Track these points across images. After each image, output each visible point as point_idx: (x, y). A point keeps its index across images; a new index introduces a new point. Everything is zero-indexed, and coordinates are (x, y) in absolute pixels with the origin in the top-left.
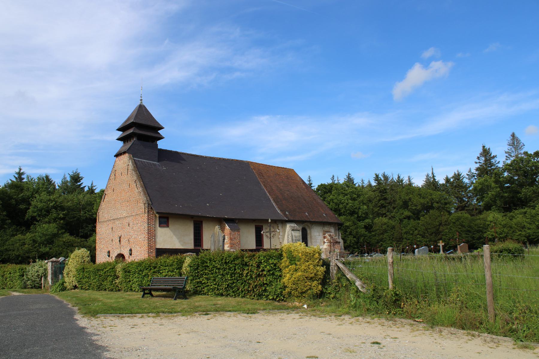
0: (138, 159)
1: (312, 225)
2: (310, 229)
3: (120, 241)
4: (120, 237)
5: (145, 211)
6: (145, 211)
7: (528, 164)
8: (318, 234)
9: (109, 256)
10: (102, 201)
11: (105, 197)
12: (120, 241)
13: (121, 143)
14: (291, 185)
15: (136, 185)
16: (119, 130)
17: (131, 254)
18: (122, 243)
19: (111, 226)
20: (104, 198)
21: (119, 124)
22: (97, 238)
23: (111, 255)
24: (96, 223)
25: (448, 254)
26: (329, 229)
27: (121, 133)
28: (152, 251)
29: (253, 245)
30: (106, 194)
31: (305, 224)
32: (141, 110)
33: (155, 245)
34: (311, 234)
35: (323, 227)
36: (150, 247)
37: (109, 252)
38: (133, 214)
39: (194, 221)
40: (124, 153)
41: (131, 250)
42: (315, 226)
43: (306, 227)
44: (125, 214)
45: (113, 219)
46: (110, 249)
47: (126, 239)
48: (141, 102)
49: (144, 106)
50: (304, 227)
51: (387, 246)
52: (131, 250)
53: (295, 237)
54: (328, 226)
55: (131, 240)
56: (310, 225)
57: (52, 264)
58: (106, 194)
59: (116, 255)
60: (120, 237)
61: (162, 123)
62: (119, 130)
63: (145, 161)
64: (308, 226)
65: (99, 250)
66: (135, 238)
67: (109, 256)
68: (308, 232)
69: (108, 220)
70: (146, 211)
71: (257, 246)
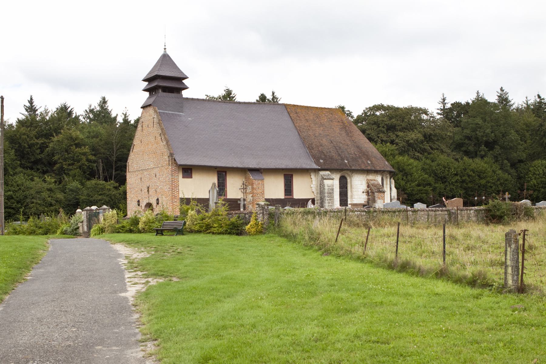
0: (163, 111)
1: (352, 173)
2: (350, 177)
3: (148, 191)
4: (148, 188)
5: (169, 163)
6: (169, 163)
7: (436, 141)
8: (360, 183)
9: (139, 205)
10: (131, 151)
11: (133, 147)
12: (148, 191)
13: (147, 94)
14: (333, 129)
15: (161, 138)
16: (145, 80)
17: (158, 204)
18: (150, 193)
19: (139, 176)
20: (133, 149)
21: (144, 75)
22: (127, 187)
23: (141, 204)
24: (126, 173)
25: (431, 208)
26: (374, 177)
27: (147, 83)
28: (176, 200)
29: (280, 194)
30: (134, 145)
31: (343, 172)
32: (165, 59)
33: (179, 196)
34: (351, 183)
35: (367, 175)
36: (174, 197)
37: (139, 201)
38: (159, 166)
39: (218, 172)
40: (150, 105)
41: (158, 200)
42: (356, 174)
43: (346, 176)
44: (152, 166)
45: (142, 170)
46: (140, 198)
47: (153, 189)
48: (165, 52)
49: (168, 56)
50: (343, 175)
51: (417, 197)
52: (158, 200)
53: (328, 187)
54: (373, 174)
55: (158, 190)
56: (350, 173)
57: (87, 212)
58: (134, 145)
59: (145, 204)
60: (148, 188)
61: (186, 73)
62: (145, 80)
63: (170, 112)
64: (347, 174)
65: (130, 199)
66: (161, 188)
67: (139, 205)
68: (349, 181)
69: (137, 171)
70: (170, 163)
71: (285, 195)
